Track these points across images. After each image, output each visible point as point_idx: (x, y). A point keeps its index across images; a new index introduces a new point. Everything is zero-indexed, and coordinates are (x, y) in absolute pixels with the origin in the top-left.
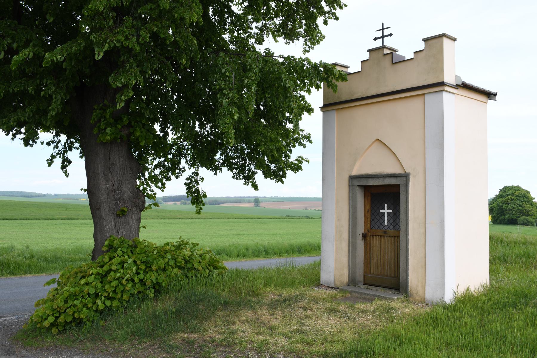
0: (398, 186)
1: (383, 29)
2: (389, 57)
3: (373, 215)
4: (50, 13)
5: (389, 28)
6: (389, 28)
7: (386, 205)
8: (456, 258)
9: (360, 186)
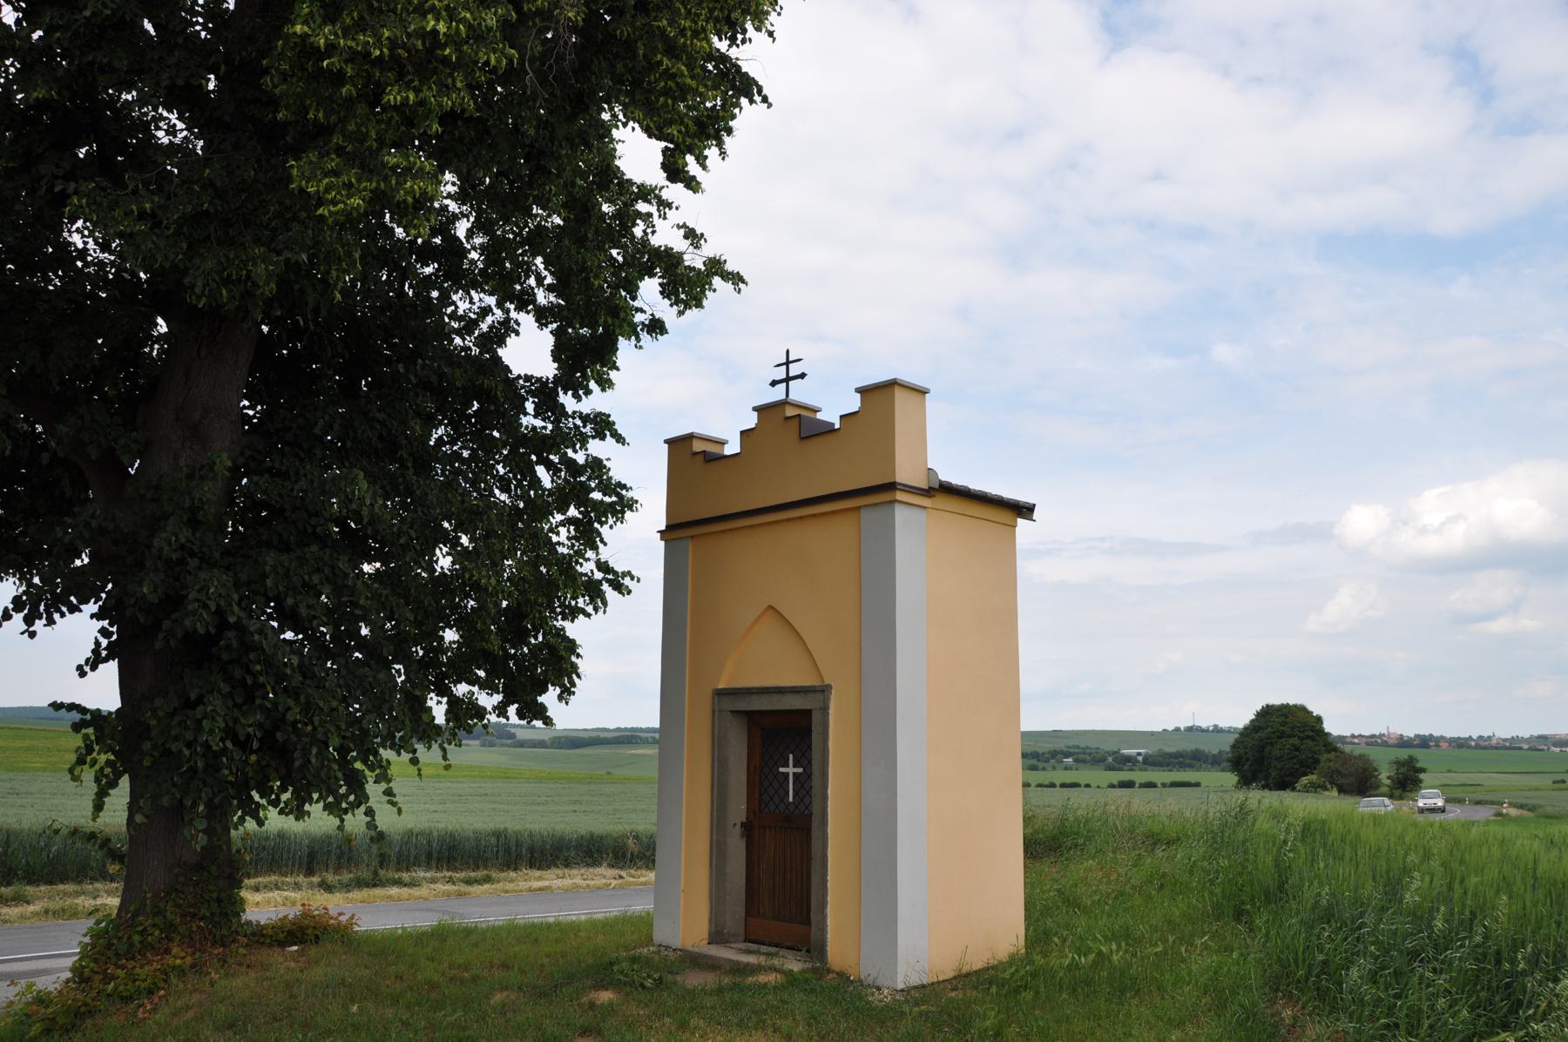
0: (807, 714)
1: (788, 363)
2: (796, 421)
3: (762, 780)
4: (615, 287)
8: (938, 886)
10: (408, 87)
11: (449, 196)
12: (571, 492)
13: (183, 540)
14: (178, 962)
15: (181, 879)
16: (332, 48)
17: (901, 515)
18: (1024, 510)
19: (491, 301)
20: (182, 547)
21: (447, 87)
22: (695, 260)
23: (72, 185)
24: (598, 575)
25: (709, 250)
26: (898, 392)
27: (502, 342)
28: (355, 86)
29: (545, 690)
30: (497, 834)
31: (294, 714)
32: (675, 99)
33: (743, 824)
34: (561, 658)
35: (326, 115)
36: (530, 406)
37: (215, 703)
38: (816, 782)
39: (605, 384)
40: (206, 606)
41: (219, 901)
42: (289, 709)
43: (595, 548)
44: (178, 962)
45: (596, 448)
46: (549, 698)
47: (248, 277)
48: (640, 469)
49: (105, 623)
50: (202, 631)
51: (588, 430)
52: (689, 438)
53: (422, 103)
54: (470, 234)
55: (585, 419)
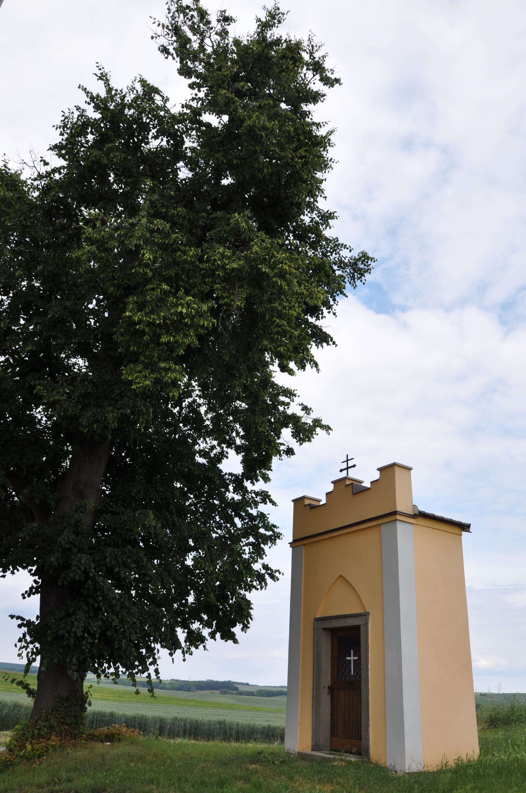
1: (347, 461)
3: (339, 665)
5: (353, 459)
6: (353, 459)
7: (352, 651)
9: (324, 629)
10: (171, 335)
11: (197, 395)
12: (250, 530)
13: (71, 539)
14: (54, 743)
15: (59, 704)
16: (140, 321)
17: (400, 527)
18: (465, 527)
19: (215, 443)
20: (71, 543)
21: (187, 335)
22: (308, 420)
23: (38, 382)
24: (263, 571)
25: (314, 415)
26: (396, 469)
27: (220, 461)
28: (149, 336)
29: (235, 625)
30: (220, 723)
31: (116, 622)
32: (281, 336)
33: (329, 687)
34: (243, 609)
35: (138, 349)
36: (231, 488)
37: (81, 615)
38: (363, 662)
39: (266, 479)
40: (80, 568)
41: (75, 717)
42: (113, 620)
43: (262, 558)
44: (54, 743)
45: (262, 508)
46: (237, 629)
47: (105, 419)
48: (281, 516)
49: (36, 578)
50: (77, 579)
51: (258, 499)
52: (303, 498)
53: (176, 342)
54: (206, 412)
55: (257, 494)
